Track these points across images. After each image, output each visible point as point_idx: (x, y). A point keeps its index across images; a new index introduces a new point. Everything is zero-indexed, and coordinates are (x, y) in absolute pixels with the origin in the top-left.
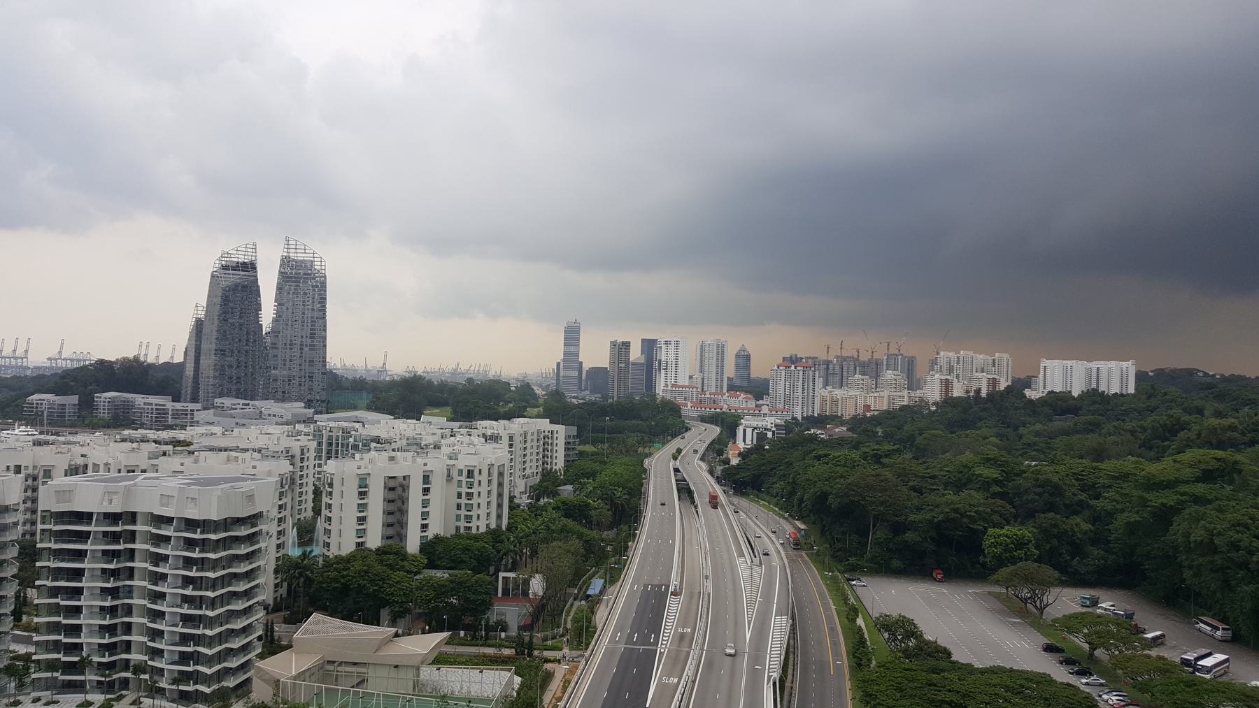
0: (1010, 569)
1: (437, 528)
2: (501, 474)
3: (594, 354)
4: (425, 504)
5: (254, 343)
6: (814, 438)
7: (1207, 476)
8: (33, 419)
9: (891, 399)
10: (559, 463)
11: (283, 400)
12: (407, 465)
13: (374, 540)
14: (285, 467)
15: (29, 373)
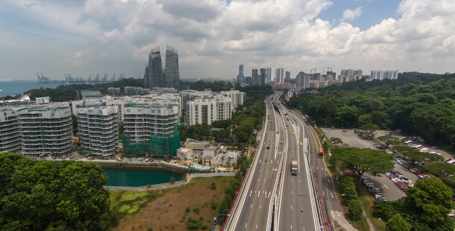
0: (365, 125)
1: (215, 119)
2: (230, 104)
3: (248, 73)
4: (212, 112)
5: (160, 73)
6: (309, 94)
7: (422, 100)
8: (111, 94)
9: (329, 83)
10: (242, 103)
12: (207, 103)
15: (100, 83)
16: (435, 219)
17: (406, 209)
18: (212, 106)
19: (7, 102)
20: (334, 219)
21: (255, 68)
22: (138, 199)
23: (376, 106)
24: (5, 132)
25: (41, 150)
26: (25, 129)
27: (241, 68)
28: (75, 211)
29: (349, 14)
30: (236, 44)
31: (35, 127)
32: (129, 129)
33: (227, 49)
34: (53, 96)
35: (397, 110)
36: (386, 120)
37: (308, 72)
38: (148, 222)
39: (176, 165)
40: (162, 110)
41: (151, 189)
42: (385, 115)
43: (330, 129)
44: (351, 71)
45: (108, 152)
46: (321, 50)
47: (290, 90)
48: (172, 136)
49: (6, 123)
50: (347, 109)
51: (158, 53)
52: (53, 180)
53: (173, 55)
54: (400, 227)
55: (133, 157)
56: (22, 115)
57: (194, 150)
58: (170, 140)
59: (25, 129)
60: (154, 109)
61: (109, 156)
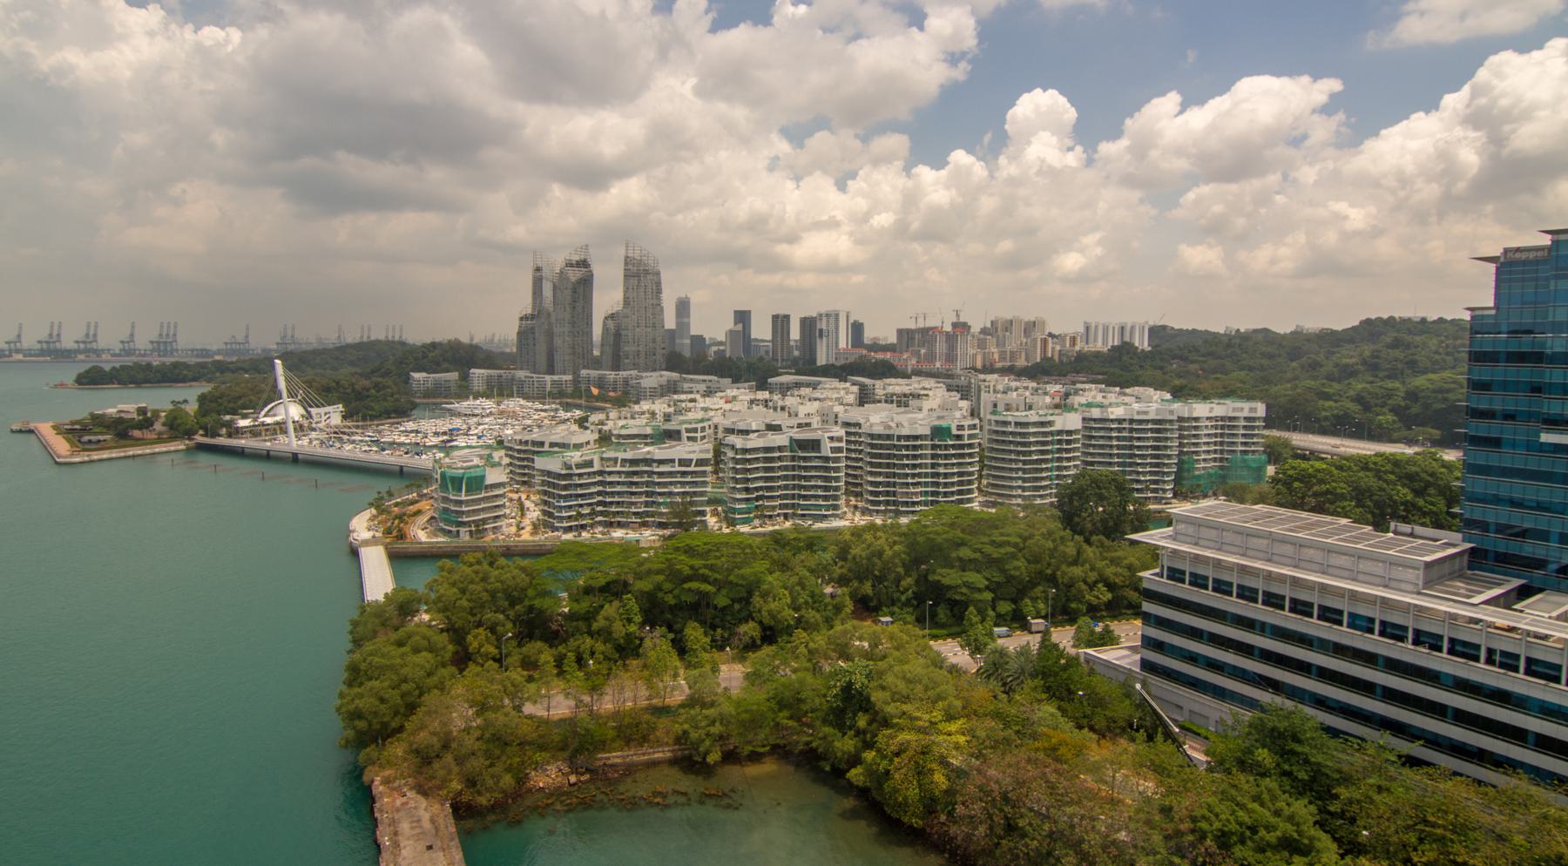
21: (782, 312)
27: (743, 317)
53: (647, 272)
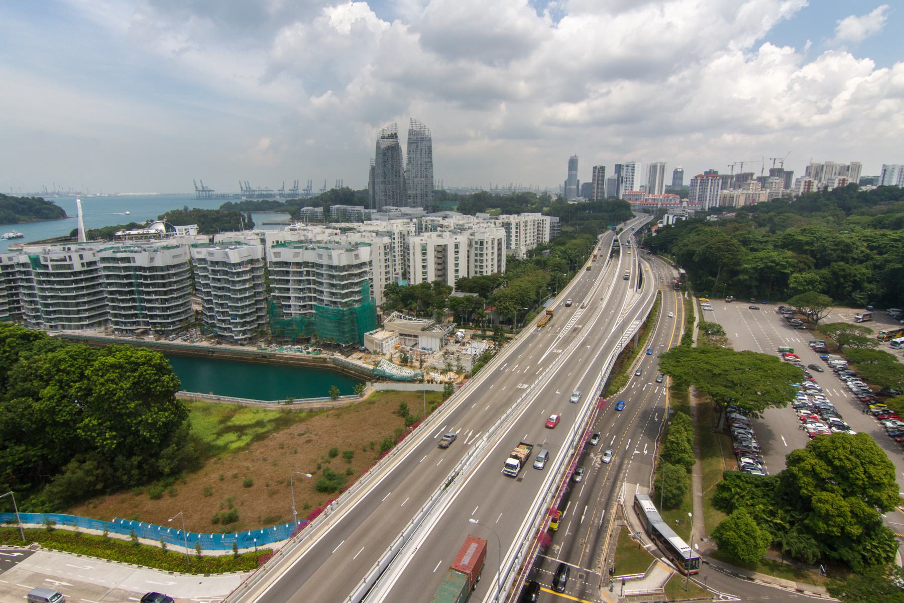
1: (463, 273)
4: (457, 259)
5: (399, 178)
10: (547, 238)
11: (414, 207)
12: (448, 240)
13: (431, 278)
14: (386, 240)
16: (835, 529)
17: (783, 499)
18: (456, 246)
19: (129, 234)
20: (622, 501)
22: (260, 424)
23: (843, 251)
24: (83, 288)
25: (138, 323)
26: (110, 284)
27: (573, 163)
28: (109, 440)
29: (852, 27)
30: (571, 111)
31: (125, 281)
32: (279, 289)
33: (551, 122)
34: (203, 223)
35: (889, 261)
36: (866, 285)
37: (723, 171)
38: (252, 469)
39: (360, 363)
40: (335, 254)
41: (292, 407)
42: (864, 274)
43: (723, 302)
44: (830, 166)
45: (244, 332)
46: (768, 117)
47: (670, 211)
48: (357, 306)
49: (85, 272)
50: (767, 258)
51: (394, 136)
52: (75, 382)
53: (423, 139)
54: (740, 537)
55: (286, 343)
56: (104, 260)
57: (401, 335)
58: (352, 313)
59: (110, 284)
60: (321, 251)
61: (245, 339)
